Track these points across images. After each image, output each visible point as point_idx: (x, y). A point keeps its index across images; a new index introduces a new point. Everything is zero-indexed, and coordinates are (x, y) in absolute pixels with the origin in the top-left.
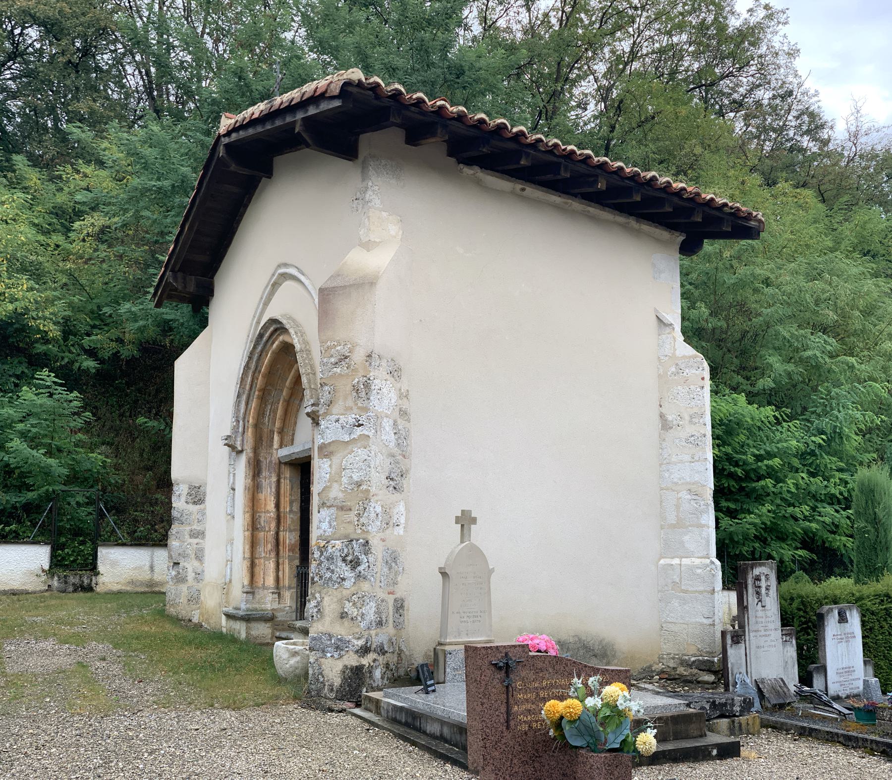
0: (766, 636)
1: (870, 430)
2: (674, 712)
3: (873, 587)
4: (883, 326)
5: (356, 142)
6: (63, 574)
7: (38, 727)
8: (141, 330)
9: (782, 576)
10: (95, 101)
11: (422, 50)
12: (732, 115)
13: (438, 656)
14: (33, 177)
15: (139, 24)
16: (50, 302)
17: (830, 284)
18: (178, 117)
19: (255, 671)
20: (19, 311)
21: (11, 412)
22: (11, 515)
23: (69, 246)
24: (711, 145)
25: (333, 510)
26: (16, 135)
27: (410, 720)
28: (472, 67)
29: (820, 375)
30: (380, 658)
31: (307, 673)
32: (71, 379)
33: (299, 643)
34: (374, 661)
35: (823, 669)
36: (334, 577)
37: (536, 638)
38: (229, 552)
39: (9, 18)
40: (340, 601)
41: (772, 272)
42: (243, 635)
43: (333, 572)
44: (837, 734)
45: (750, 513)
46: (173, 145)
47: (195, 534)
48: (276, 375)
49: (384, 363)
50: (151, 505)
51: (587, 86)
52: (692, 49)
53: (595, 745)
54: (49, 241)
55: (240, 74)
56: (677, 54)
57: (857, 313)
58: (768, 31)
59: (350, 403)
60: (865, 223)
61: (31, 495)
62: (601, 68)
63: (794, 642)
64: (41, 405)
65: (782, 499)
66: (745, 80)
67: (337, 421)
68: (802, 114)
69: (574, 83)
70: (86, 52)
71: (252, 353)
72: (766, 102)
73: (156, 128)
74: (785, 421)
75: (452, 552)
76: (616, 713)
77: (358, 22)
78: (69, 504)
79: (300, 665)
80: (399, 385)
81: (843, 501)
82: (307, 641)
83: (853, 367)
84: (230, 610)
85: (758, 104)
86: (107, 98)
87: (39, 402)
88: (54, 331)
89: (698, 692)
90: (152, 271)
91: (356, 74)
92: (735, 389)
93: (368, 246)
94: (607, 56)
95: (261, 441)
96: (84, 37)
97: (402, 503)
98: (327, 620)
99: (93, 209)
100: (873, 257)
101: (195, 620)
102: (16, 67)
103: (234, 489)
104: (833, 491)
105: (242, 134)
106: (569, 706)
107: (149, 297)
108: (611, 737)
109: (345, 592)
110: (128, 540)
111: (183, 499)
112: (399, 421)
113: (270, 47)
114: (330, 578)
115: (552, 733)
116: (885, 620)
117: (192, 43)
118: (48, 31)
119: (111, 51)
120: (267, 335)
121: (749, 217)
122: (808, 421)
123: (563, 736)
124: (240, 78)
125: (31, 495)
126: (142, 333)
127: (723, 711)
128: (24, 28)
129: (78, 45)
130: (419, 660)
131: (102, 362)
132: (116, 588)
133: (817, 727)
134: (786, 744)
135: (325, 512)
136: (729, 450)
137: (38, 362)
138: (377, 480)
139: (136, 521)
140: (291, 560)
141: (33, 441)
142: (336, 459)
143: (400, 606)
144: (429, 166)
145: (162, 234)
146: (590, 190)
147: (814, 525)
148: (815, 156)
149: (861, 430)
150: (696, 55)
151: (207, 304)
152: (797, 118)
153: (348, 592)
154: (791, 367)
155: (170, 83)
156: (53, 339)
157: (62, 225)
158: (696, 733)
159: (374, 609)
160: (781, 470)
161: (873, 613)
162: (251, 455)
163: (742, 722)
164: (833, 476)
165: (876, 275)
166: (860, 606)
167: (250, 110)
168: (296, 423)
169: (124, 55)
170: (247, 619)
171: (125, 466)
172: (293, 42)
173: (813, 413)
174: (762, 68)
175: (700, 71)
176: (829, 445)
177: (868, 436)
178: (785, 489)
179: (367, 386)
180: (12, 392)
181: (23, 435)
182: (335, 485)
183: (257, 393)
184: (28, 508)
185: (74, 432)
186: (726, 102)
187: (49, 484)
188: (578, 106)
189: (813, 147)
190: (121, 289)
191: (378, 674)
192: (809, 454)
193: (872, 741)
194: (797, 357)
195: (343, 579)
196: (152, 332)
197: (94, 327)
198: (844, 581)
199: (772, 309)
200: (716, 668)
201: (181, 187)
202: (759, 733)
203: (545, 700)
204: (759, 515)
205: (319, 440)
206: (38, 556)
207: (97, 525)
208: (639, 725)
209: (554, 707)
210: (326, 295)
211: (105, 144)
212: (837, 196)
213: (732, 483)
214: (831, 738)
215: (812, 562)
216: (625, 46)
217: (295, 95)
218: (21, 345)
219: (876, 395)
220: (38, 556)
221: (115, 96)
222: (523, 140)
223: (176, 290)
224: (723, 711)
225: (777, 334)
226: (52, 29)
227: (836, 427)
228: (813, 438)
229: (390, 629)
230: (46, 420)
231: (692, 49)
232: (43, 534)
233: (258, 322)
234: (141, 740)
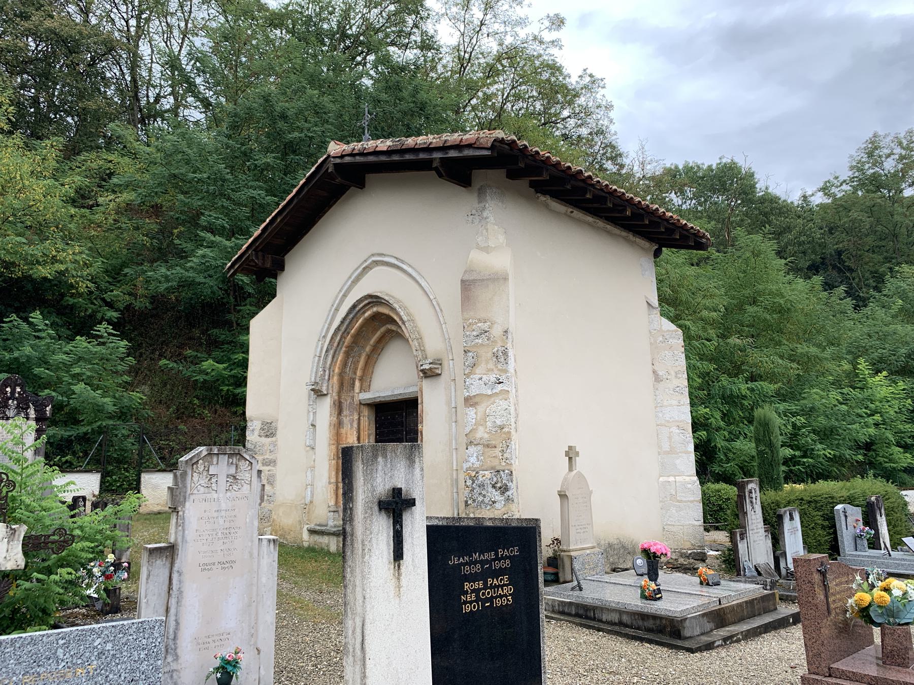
2: (757, 595)
5: (471, 174)
23: (92, 217)
25: (480, 447)
36: (486, 500)
43: (484, 496)
47: (267, 463)
59: (491, 365)
61: (83, 429)
67: (481, 379)
93: (486, 249)
95: (345, 385)
111: (256, 433)
114: (483, 501)
132: (156, 509)
142: (481, 409)
153: (499, 512)
162: (336, 398)
179: (505, 353)
182: (481, 429)
183: (344, 349)
184: (84, 439)
195: (494, 502)
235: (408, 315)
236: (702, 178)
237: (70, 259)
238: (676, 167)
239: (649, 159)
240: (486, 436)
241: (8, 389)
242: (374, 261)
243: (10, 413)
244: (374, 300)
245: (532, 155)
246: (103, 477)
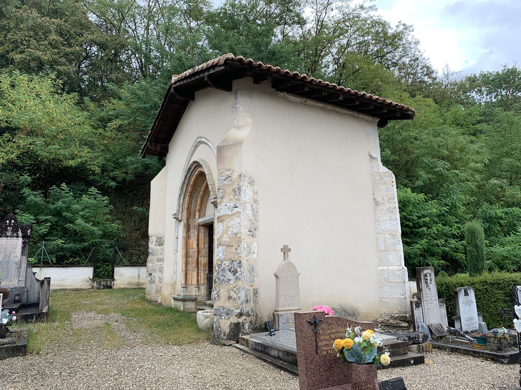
0: (431, 303)
1: (468, 204)
2: (392, 342)
3: (478, 278)
4: (469, 156)
5: (231, 83)
6: (98, 281)
7: (88, 355)
8: (136, 169)
9: (436, 274)
10: (118, 73)
11: (258, 46)
12: (393, 68)
13: (275, 317)
14: (92, 106)
15: (138, 42)
16: (96, 158)
17: (444, 138)
18: (153, 78)
19: (188, 326)
20: (83, 162)
21: (78, 206)
22: (76, 254)
23: (105, 133)
24: (386, 81)
25: (224, 247)
26: (85, 89)
27: (263, 349)
28: (279, 52)
29: (444, 179)
30: (248, 319)
31: (213, 327)
32: (104, 191)
33: (209, 312)
34: (245, 320)
35: (459, 319)
36: (225, 279)
37: (323, 307)
38: (175, 268)
39: (85, 43)
40: (228, 291)
41: (418, 134)
42: (182, 308)
43: (224, 276)
44: (469, 350)
45: (417, 243)
46: (151, 89)
47: (159, 260)
48: (197, 183)
49: (247, 179)
50: (139, 247)
51: (329, 58)
52: (373, 42)
53: (360, 361)
54: (97, 132)
55: (180, 59)
56: (368, 44)
57: (457, 151)
58: (406, 34)
59: (231, 197)
60: (456, 112)
61: (86, 244)
62: (334, 51)
63: (445, 306)
64: (91, 203)
65: (431, 236)
66: (397, 54)
67: (226, 205)
68: (424, 67)
69: (323, 57)
70: (116, 55)
71: (186, 176)
72: (407, 63)
73: (144, 83)
74: (430, 200)
75: (280, 265)
76: (369, 344)
77: (230, 36)
78: (102, 247)
79: (209, 323)
80: (253, 188)
81: (459, 237)
82: (213, 310)
83: (458, 174)
84: (176, 296)
85: (404, 64)
86: (124, 72)
87: (90, 202)
88: (98, 170)
89: (400, 332)
90: (141, 143)
91: (231, 55)
92: (405, 186)
93: (238, 127)
94: (337, 46)
95: (190, 215)
96: (115, 49)
97: (256, 243)
98: (222, 300)
99: (116, 118)
100: (462, 126)
101: (159, 301)
102: (87, 62)
103: (177, 238)
104: (454, 232)
105: (181, 83)
107: (139, 154)
108: (368, 357)
109: (230, 286)
110: (127, 263)
111: (154, 243)
112: (254, 205)
113: (193, 48)
115: (338, 355)
116: (486, 294)
117: (160, 48)
118: (101, 48)
119: (126, 54)
120: (193, 168)
121: (408, 110)
122: (440, 200)
123: (344, 357)
124: (180, 61)
125: (86, 244)
126: (136, 170)
127: (414, 341)
128: (91, 47)
129: (113, 52)
130: (266, 320)
131: (118, 182)
132: (122, 286)
133: (459, 347)
134: (445, 356)
135: (220, 248)
136: (405, 214)
137: (90, 184)
138: (244, 232)
139: (132, 254)
140: (204, 271)
141: (87, 219)
142: (225, 223)
143: (256, 292)
144: (264, 93)
145: (146, 127)
146: (337, 100)
147: (447, 249)
148: (430, 85)
149: (464, 204)
150: (375, 45)
151: (165, 156)
152: (422, 69)
154: (430, 176)
155: (150, 64)
156: (97, 173)
157: (103, 125)
158: (402, 353)
159: (244, 294)
160: (430, 223)
161: (480, 291)
162: (186, 222)
163: (424, 346)
164: (454, 226)
165: (463, 134)
166: (474, 287)
167: (185, 73)
168: (206, 207)
169: (131, 55)
170: (184, 300)
171: (127, 229)
172: (202, 46)
173: (441, 196)
174: (404, 49)
175: (377, 51)
176: (450, 211)
177: (468, 206)
178: (432, 232)
179: (239, 189)
180: (78, 197)
181: (83, 217)
182: (225, 235)
184: (85, 250)
185: (105, 214)
186: (390, 63)
187: (94, 239)
188: (325, 66)
189: (430, 81)
190: (127, 151)
191: (246, 326)
192: (442, 215)
193: (486, 353)
194: (432, 171)
195: (230, 280)
196: (140, 169)
197: (115, 168)
198: (463, 275)
199: (420, 150)
200: (408, 319)
201: (154, 106)
202: (432, 351)
203: (334, 339)
204: (422, 244)
205: (217, 215)
206: (88, 272)
207: (114, 257)
208: (380, 350)
209: (339, 343)
210: (220, 149)
211: (122, 91)
212: (442, 101)
213: (408, 229)
214: (466, 353)
215: (447, 266)
216: (344, 42)
217: (204, 65)
218: (83, 176)
219: (470, 188)
220: (88, 272)
221: (127, 71)
222: (305, 80)
223: (152, 150)
224: (414, 341)
225: (422, 161)
226: (102, 46)
227: (453, 202)
228: (443, 208)
229: (252, 304)
230: (93, 210)
231: (373, 42)
232: (90, 262)
233: (188, 163)
234: (135, 361)
235: (210, 171)
236: (493, 80)
237: (78, 156)
238: (475, 75)
239: (451, 72)
240: (228, 240)
241: (8, 221)
242: (199, 142)
243: (9, 234)
244: (195, 162)
245: (257, 67)
246: (95, 269)
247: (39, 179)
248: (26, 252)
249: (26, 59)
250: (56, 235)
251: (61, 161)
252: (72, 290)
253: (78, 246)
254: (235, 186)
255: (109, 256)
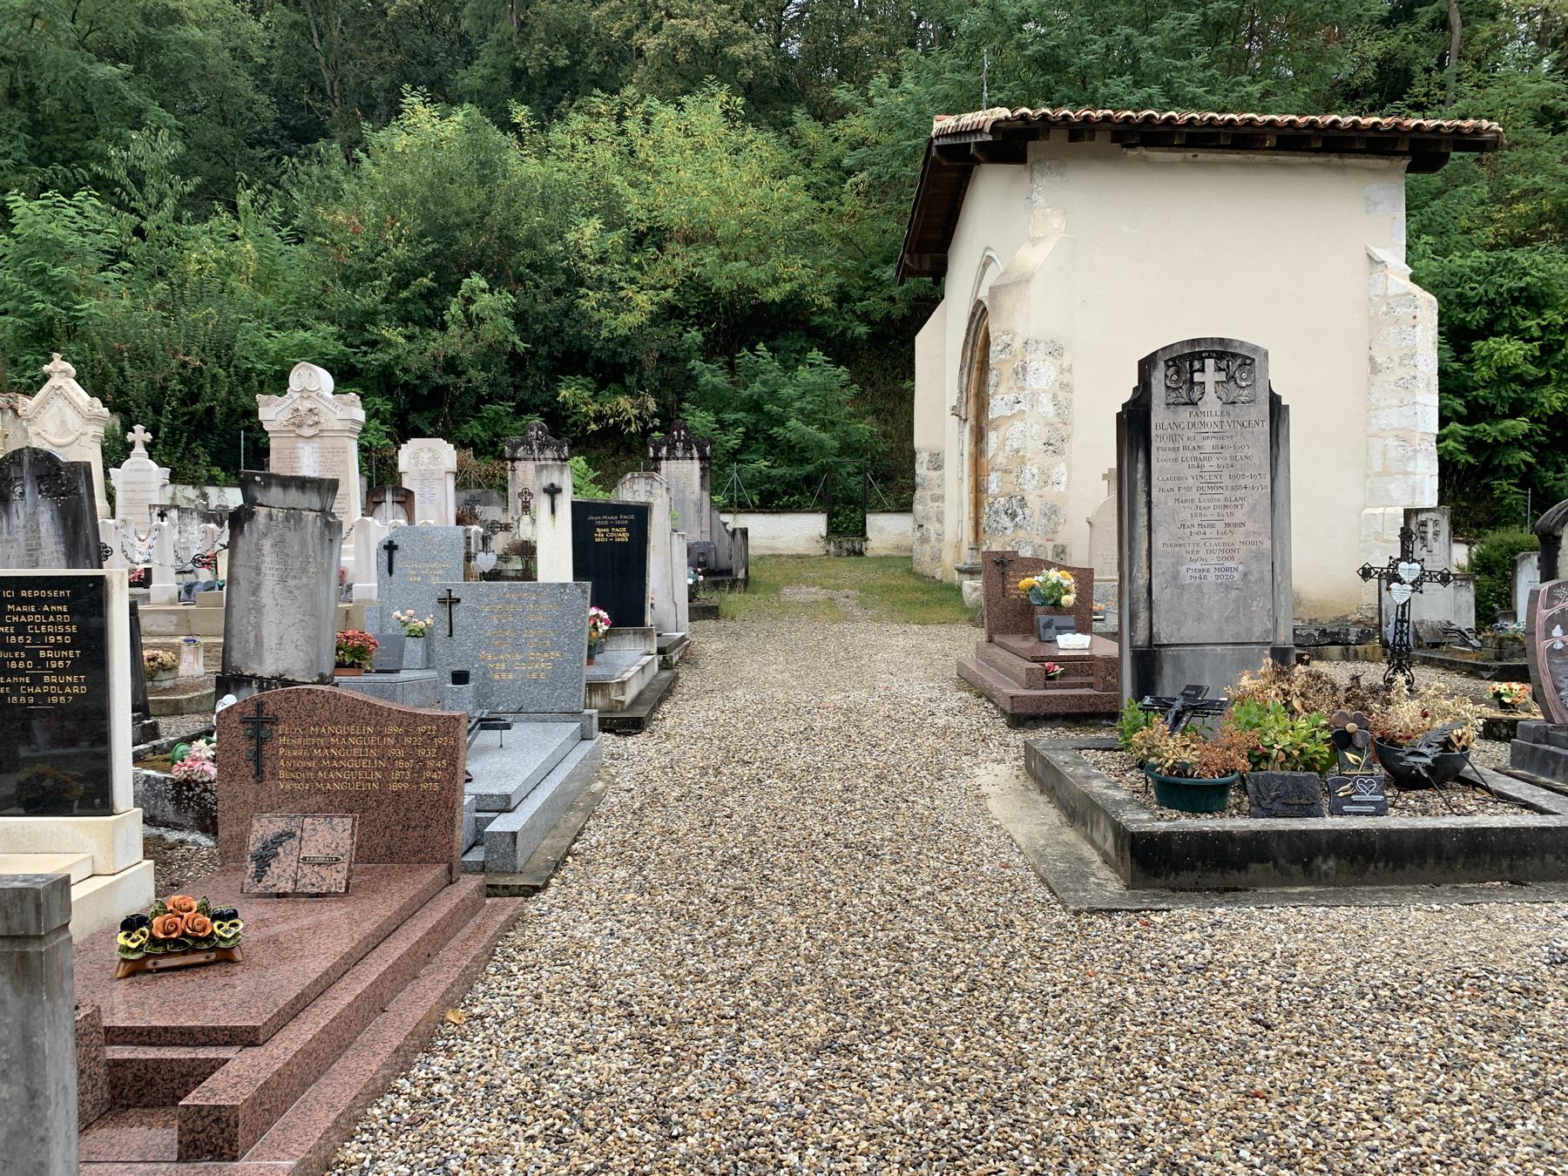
22: (795, 488)
59: (1011, 384)
61: (810, 468)
84: (960, 565)
88: (827, 302)
101: (938, 577)
106: (1036, 580)
125: (810, 468)
132: (883, 553)
141: (808, 417)
142: (1001, 431)
179: (1024, 369)
184: (809, 480)
197: (867, 289)
220: (815, 524)
237: (787, 275)
246: (829, 518)
247: (717, 331)
248: (708, 484)
249: (666, 45)
250: (756, 451)
251: (753, 291)
252: (792, 556)
253: (798, 472)
254: (1018, 363)
255: (853, 491)
